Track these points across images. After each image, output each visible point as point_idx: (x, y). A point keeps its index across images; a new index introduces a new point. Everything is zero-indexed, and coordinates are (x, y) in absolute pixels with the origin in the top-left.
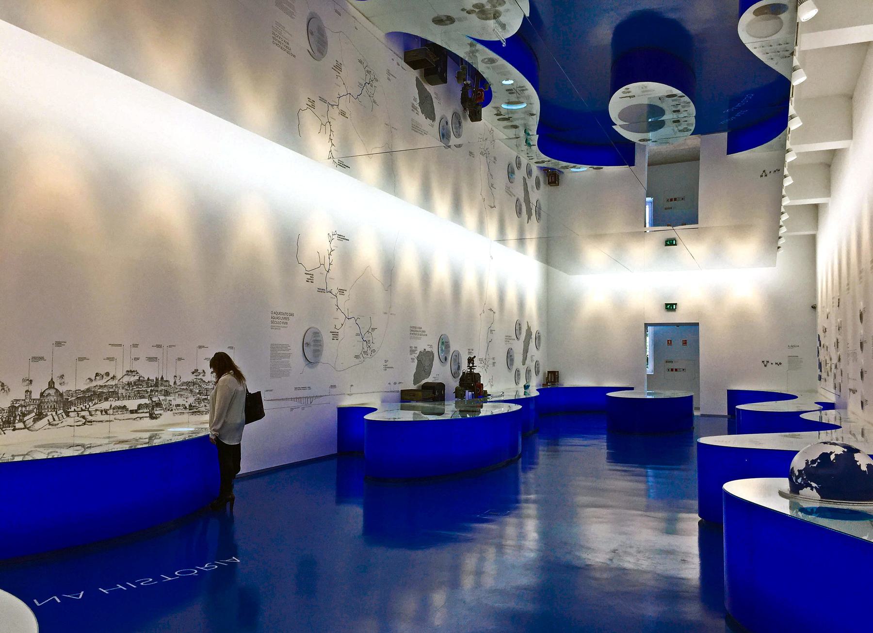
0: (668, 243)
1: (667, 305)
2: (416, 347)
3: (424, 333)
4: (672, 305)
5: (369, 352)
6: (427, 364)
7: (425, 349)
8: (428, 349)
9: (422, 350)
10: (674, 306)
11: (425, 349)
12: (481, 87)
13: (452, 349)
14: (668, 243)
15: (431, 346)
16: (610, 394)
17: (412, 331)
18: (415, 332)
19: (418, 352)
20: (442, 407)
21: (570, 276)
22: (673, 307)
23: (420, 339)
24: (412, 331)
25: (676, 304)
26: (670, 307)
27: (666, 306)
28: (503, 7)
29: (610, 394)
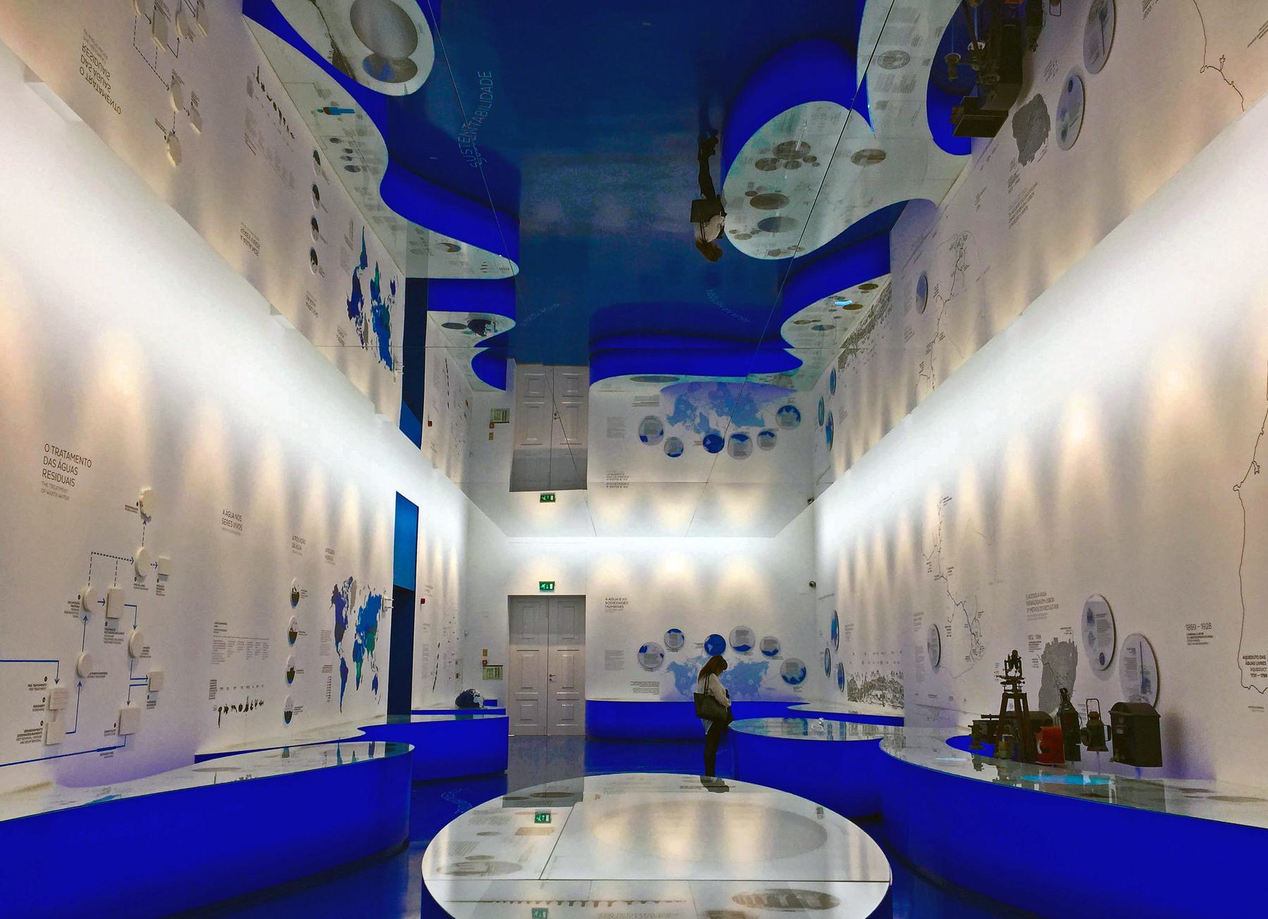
0: (544, 499)
1: (541, 583)
2: (1039, 637)
3: (1051, 604)
4: (548, 583)
5: (978, 650)
6: (1062, 670)
7: (1056, 639)
8: (1063, 638)
9: (1050, 641)
10: (551, 585)
11: (1056, 639)
12: (955, 52)
13: (1124, 633)
14: (544, 499)
15: (1068, 630)
16: (790, 708)
17: (1031, 603)
18: (1036, 604)
19: (1043, 646)
20: (1003, 753)
21: (516, 539)
22: (549, 587)
23: (1044, 617)
24: (1031, 603)
25: (553, 583)
26: (546, 586)
27: (541, 585)
28: (362, 69)
29: (790, 708)
